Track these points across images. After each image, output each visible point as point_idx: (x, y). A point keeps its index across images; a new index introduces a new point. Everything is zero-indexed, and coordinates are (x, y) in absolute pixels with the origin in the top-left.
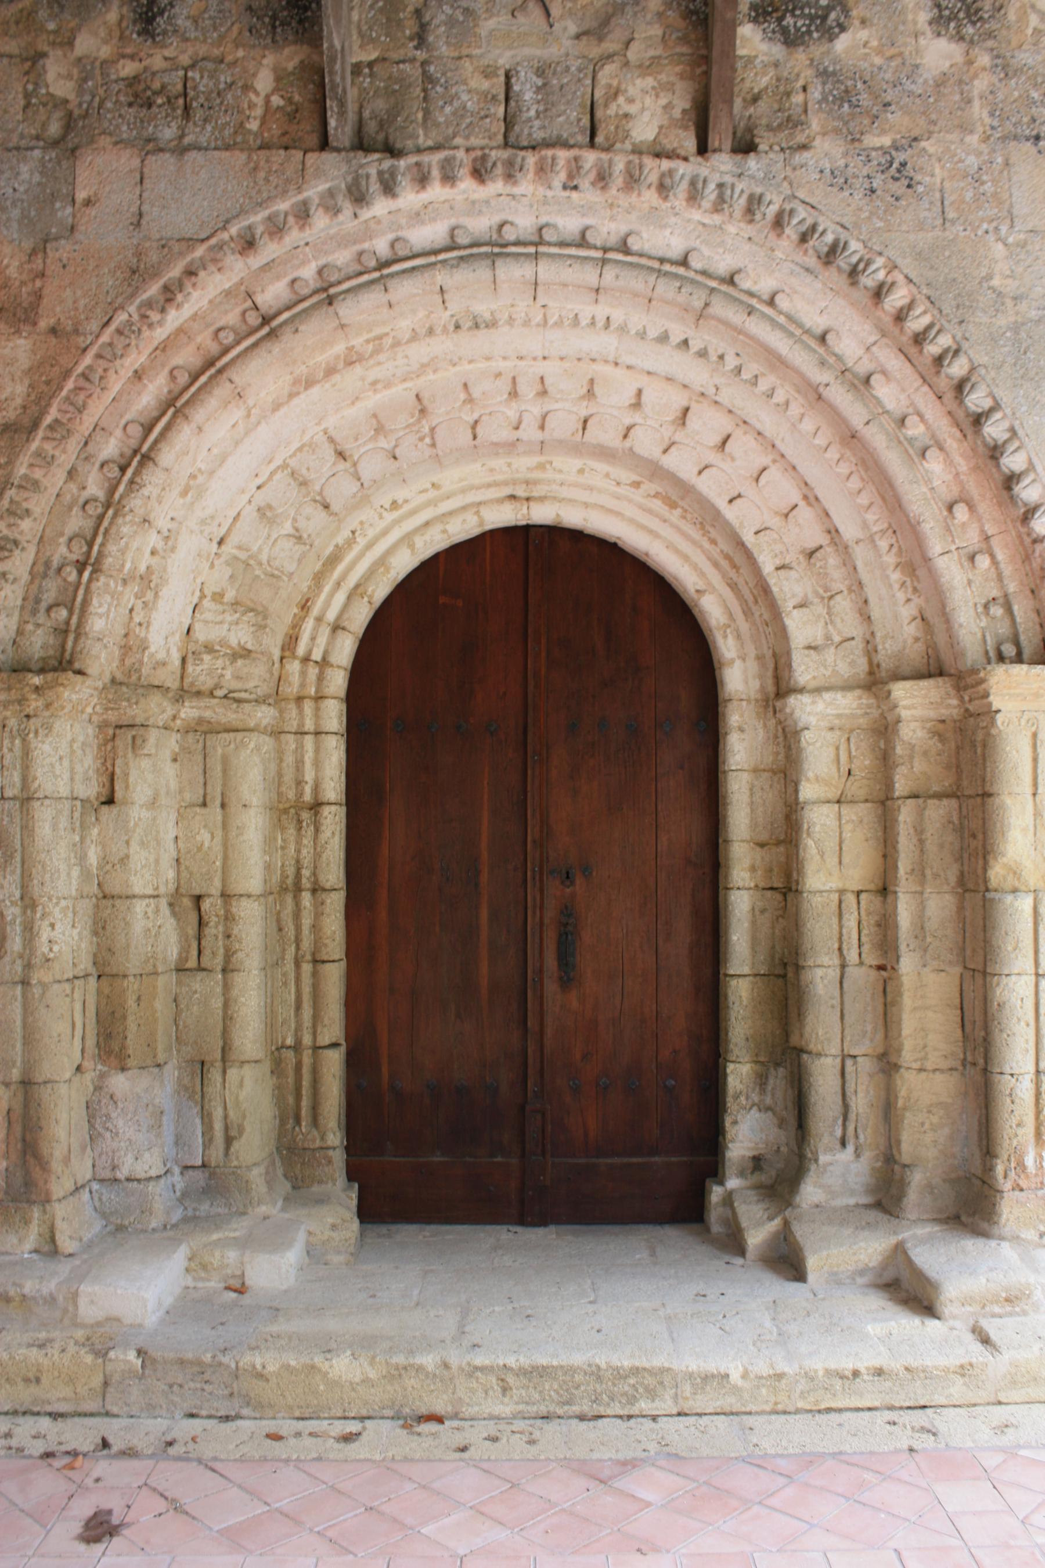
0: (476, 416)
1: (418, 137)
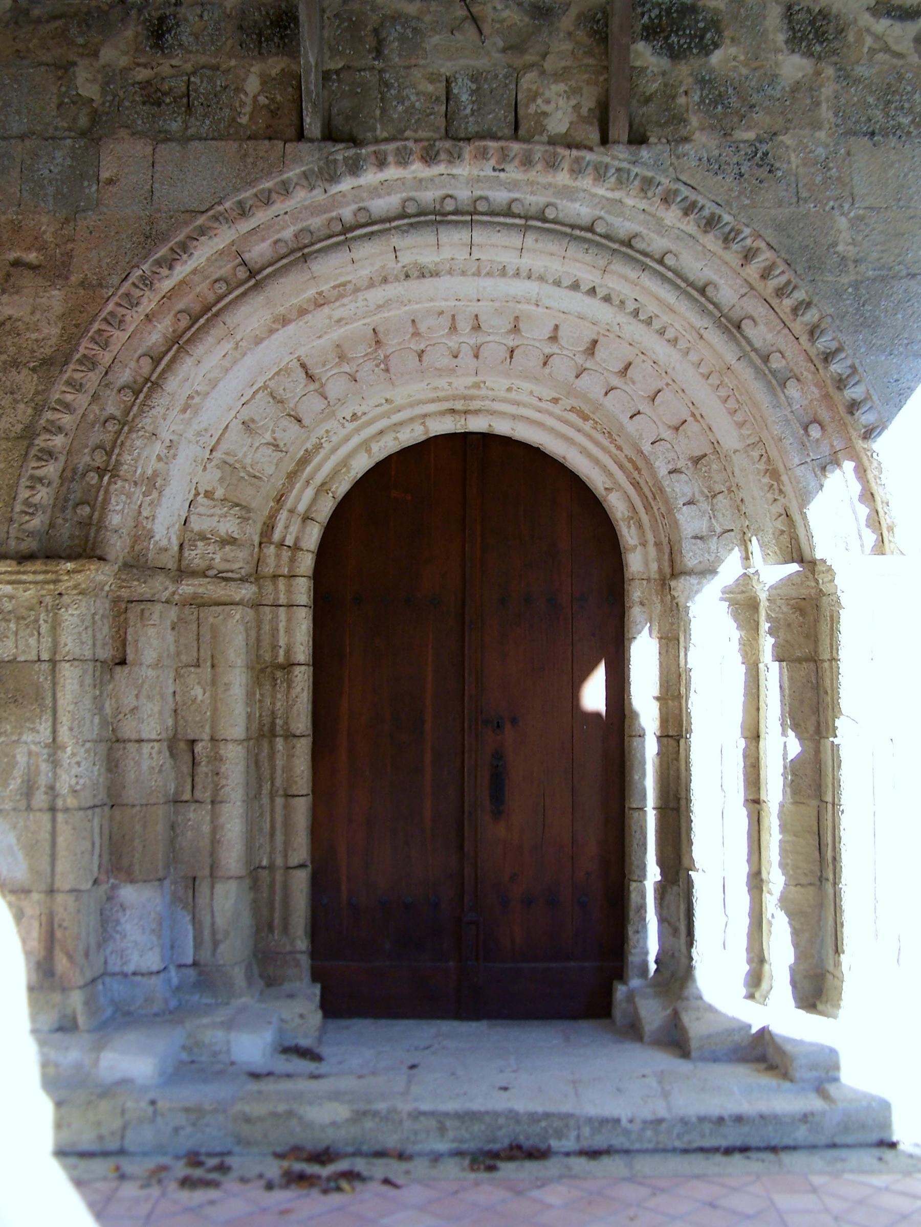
0: (422, 347)
1: (375, 131)
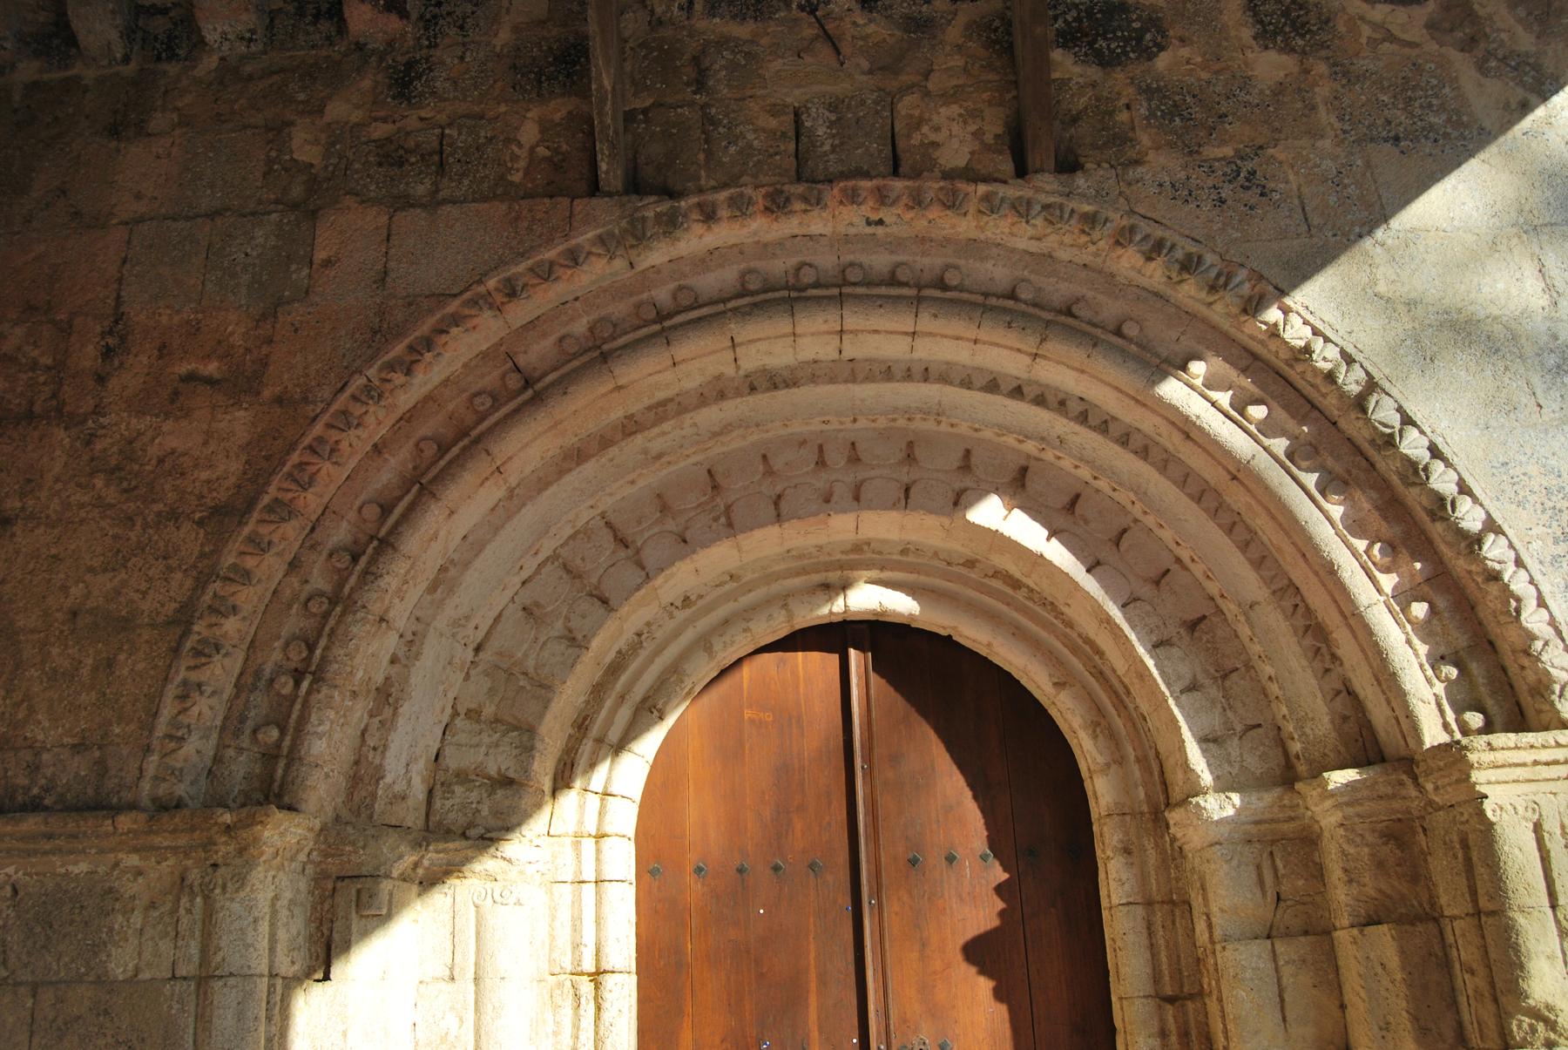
0: (779, 489)
